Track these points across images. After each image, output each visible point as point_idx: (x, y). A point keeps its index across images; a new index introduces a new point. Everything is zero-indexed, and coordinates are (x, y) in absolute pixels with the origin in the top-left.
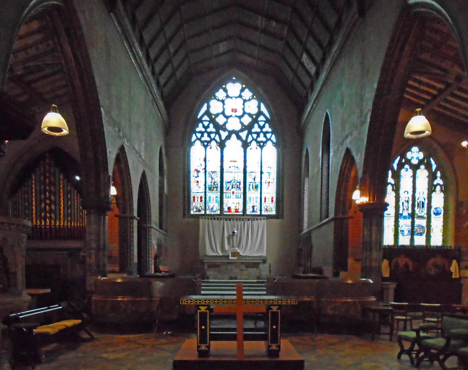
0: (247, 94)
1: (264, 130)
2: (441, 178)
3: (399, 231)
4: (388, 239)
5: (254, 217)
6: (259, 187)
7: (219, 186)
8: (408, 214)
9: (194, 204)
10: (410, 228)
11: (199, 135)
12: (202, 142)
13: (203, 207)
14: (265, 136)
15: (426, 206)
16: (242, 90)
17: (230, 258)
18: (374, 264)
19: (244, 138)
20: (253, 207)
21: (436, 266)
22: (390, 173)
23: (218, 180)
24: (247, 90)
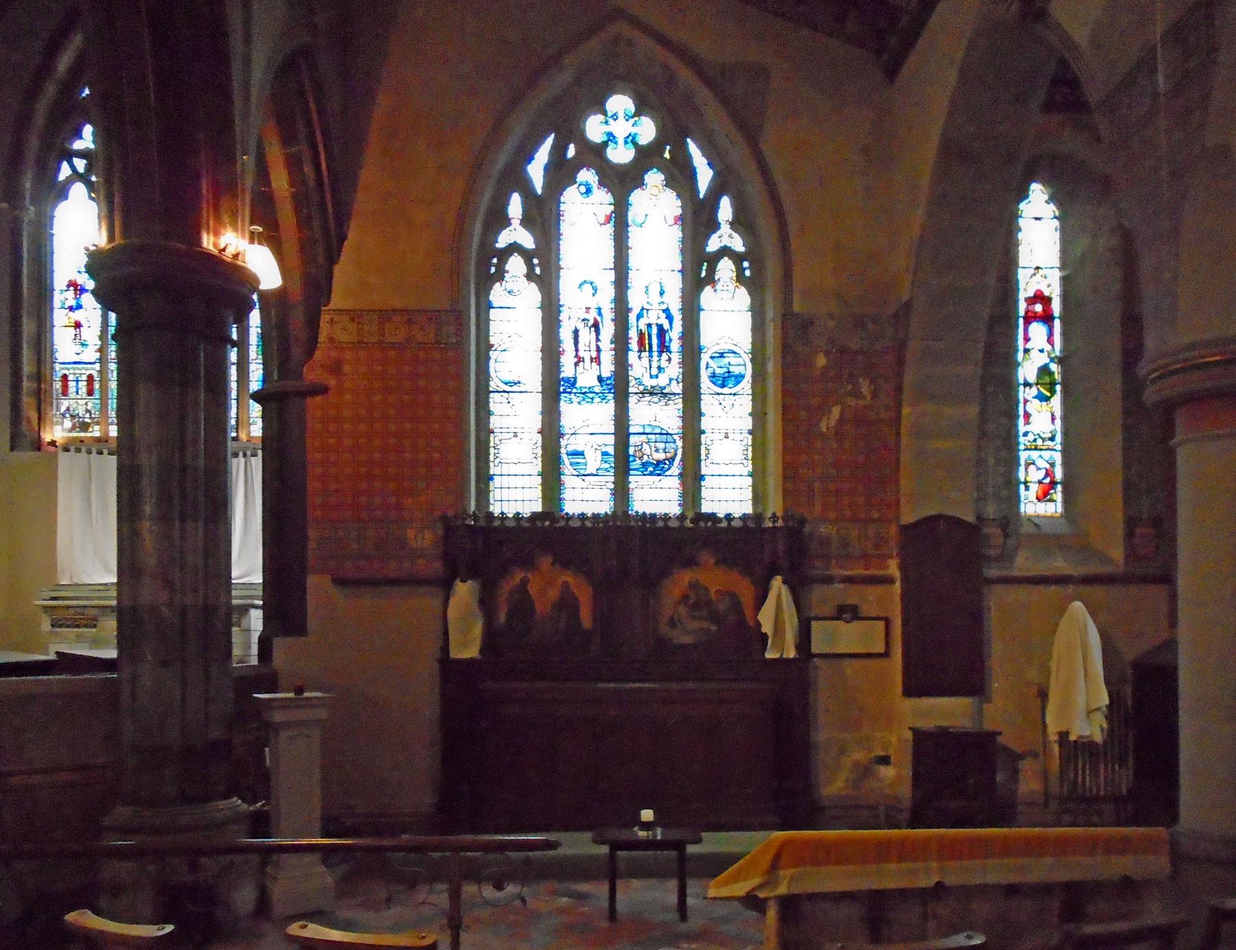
3: (564, 456)
4: (514, 492)
8: (600, 379)
9: (65, 404)
10: (611, 440)
21: (698, 602)
22: (515, 207)
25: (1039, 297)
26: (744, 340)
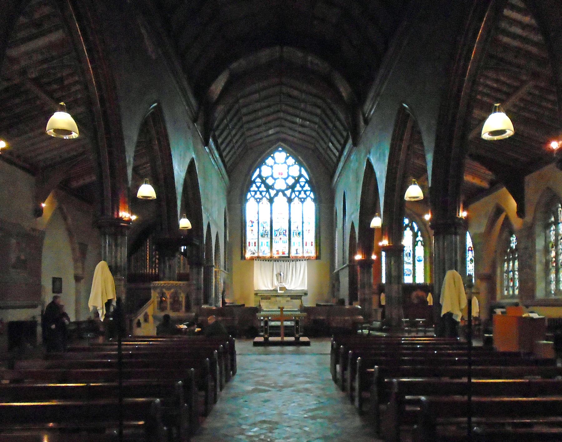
0: (291, 161)
1: (304, 189)
2: (421, 236)
5: (296, 259)
6: (301, 234)
7: (269, 233)
11: (253, 193)
12: (256, 199)
13: (257, 251)
14: (305, 193)
15: (411, 255)
16: (287, 158)
17: (279, 292)
18: (366, 296)
19: (289, 196)
20: (297, 250)
21: (418, 297)
23: (268, 229)
24: (290, 158)
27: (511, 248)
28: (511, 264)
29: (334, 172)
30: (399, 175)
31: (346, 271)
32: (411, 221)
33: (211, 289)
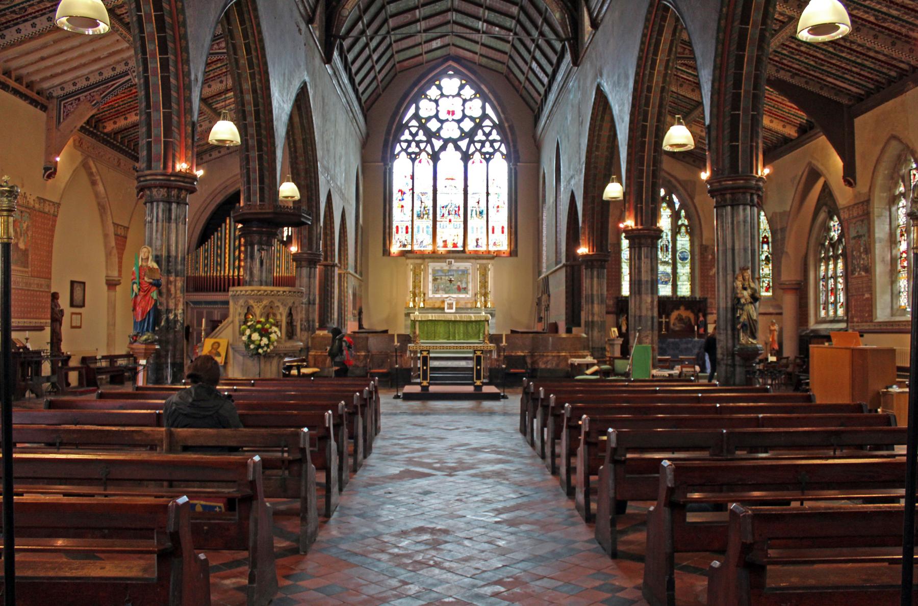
0: (468, 92)
6: (485, 214)
12: (409, 154)
13: (410, 241)
14: (492, 146)
16: (462, 87)
18: (596, 318)
19: (464, 149)
20: (477, 240)
21: (680, 319)
23: (429, 204)
24: (467, 87)
25: (765, 237)
26: (688, 246)
27: (831, 239)
28: (831, 266)
29: (541, 109)
30: (652, 110)
31: (562, 275)
32: (669, 193)
33: (332, 303)
